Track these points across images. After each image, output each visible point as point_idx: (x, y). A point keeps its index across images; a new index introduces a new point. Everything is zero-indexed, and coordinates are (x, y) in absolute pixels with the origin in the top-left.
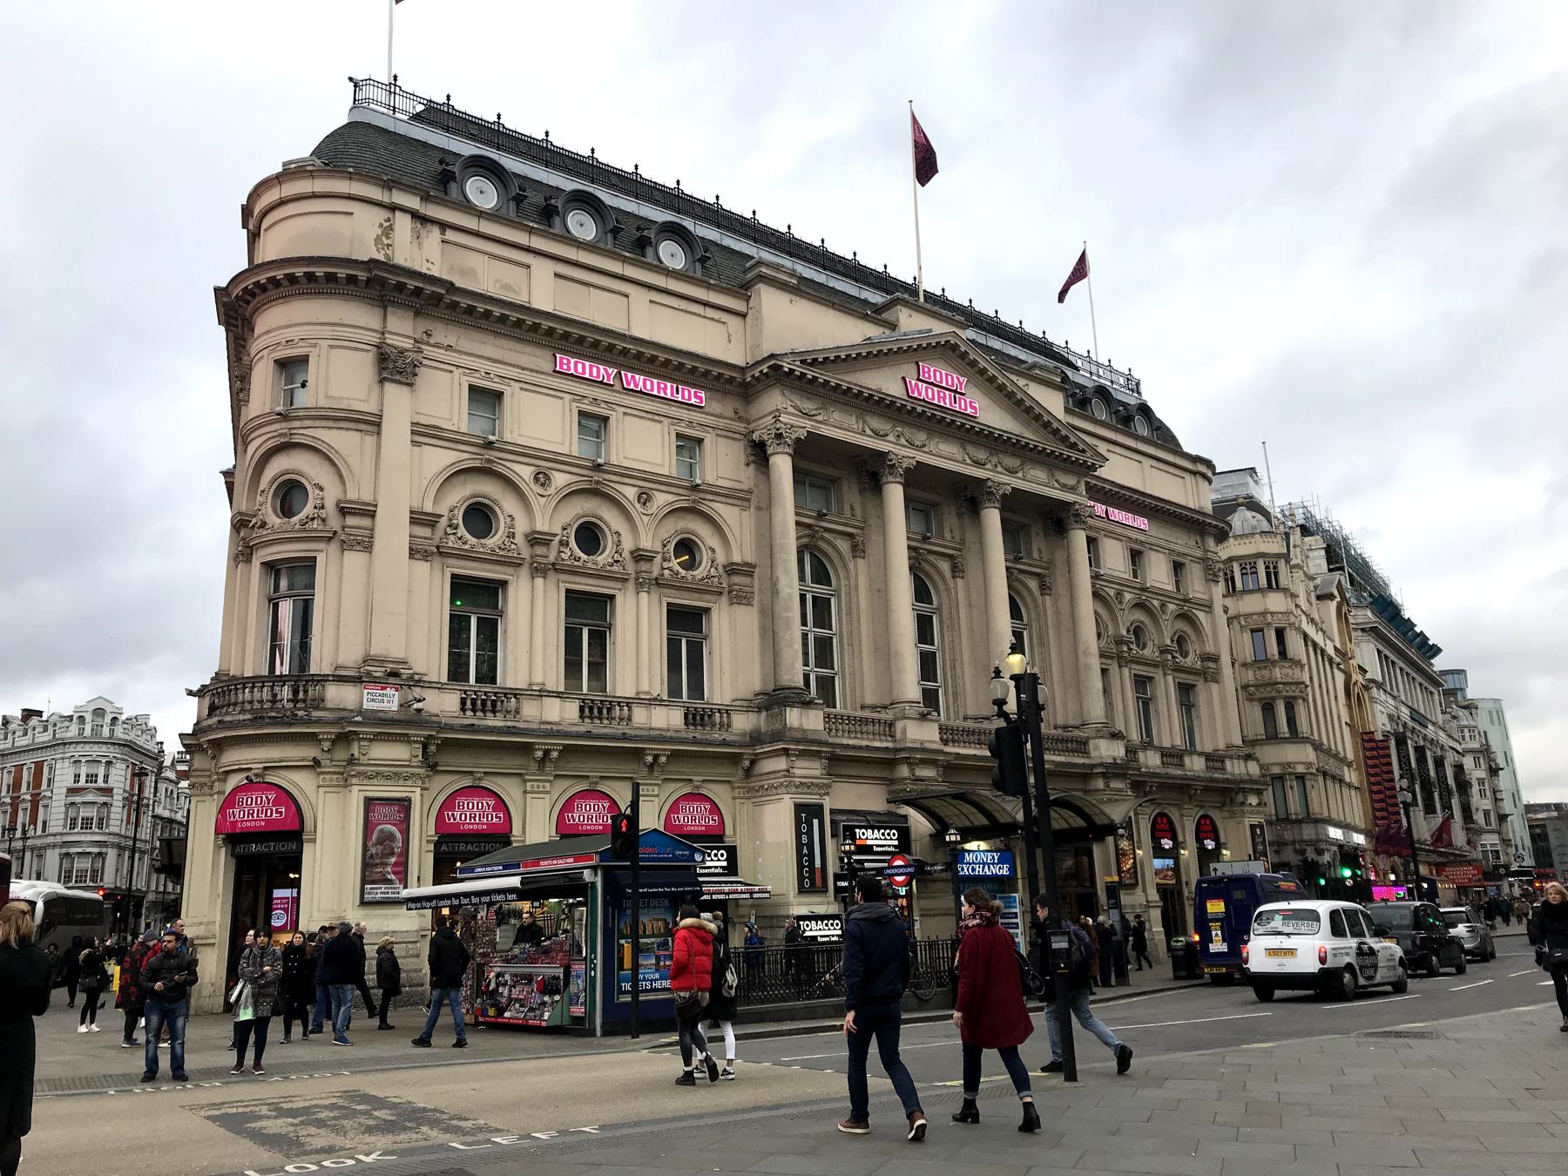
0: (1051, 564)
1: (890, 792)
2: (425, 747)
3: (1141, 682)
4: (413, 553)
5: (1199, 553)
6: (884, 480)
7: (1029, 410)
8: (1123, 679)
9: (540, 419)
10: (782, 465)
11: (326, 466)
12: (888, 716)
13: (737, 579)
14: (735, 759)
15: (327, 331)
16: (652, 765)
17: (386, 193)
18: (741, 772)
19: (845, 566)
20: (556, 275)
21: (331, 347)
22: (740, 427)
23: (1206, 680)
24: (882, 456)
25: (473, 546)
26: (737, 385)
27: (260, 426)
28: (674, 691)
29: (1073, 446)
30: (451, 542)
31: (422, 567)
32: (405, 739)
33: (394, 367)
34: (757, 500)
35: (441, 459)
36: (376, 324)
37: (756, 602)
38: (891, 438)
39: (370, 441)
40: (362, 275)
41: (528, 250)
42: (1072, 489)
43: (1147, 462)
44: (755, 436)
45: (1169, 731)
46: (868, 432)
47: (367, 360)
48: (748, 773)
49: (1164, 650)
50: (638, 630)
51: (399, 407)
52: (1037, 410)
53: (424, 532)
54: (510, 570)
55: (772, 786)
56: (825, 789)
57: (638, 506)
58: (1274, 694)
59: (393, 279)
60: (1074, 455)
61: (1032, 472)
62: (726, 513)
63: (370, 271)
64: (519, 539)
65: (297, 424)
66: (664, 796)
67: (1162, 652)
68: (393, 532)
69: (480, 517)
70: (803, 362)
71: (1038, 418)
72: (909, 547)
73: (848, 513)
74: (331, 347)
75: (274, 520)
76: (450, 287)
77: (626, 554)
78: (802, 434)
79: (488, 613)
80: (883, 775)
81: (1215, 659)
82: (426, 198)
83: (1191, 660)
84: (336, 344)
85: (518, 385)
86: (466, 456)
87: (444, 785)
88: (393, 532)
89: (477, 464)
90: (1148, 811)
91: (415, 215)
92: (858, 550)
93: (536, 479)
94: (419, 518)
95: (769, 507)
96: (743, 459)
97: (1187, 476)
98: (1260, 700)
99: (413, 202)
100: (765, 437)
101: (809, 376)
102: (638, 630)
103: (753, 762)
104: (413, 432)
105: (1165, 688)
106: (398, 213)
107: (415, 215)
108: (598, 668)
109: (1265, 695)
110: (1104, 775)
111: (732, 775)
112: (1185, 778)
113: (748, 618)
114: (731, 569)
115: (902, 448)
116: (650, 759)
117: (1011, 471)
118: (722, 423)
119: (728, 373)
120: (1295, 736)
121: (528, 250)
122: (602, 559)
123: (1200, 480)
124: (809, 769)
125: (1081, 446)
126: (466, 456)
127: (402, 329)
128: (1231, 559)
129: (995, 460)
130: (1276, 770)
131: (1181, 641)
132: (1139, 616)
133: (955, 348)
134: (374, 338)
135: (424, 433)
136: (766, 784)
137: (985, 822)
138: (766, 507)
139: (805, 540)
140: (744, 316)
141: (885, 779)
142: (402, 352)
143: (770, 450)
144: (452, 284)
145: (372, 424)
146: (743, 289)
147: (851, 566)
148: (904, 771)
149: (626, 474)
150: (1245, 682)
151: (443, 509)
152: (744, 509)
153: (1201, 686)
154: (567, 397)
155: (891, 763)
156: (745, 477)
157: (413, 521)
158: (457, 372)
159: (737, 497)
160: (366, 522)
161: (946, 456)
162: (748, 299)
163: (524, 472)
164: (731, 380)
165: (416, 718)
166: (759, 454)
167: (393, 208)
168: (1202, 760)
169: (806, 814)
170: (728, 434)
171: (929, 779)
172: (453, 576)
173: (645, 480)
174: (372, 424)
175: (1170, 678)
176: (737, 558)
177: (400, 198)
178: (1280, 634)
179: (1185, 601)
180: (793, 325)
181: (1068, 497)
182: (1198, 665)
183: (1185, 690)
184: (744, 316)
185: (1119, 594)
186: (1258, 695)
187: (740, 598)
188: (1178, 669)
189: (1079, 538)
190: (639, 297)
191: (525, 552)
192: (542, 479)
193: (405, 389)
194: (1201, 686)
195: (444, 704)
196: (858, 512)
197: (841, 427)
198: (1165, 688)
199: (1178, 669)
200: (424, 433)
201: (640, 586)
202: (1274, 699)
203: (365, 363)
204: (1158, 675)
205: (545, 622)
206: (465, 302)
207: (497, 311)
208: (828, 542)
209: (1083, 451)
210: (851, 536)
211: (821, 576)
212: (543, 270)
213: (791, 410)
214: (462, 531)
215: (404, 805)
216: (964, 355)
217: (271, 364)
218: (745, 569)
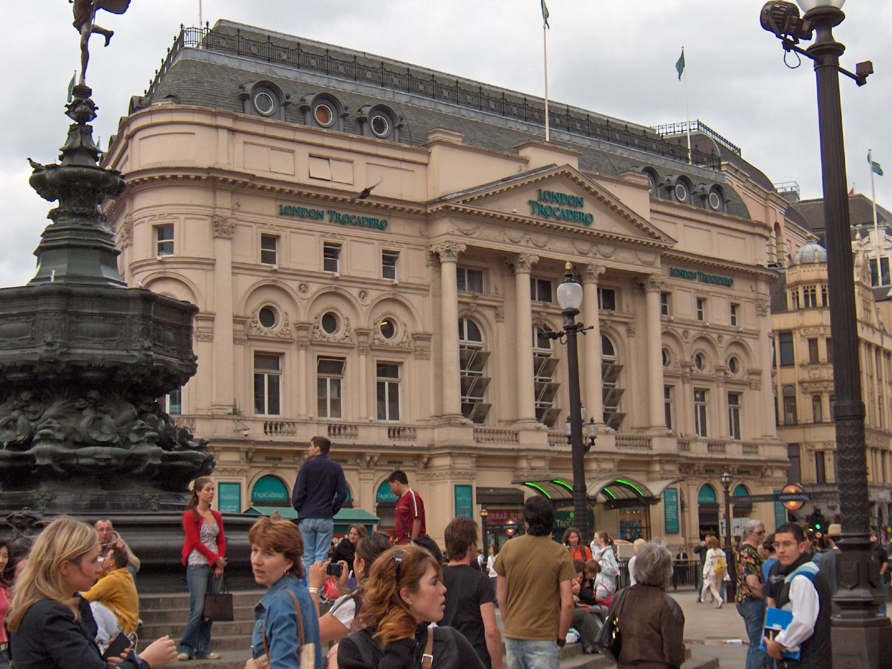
0: (634, 316)
1: (515, 476)
2: (247, 453)
3: (701, 394)
4: (235, 340)
5: (753, 295)
6: (517, 271)
7: (620, 212)
8: (684, 393)
9: (301, 248)
10: (449, 270)
11: (185, 290)
12: (515, 427)
13: (419, 343)
14: (418, 457)
15: (183, 209)
16: (369, 463)
17: (213, 118)
18: (422, 465)
19: (490, 327)
20: (311, 156)
21: (186, 218)
22: (422, 241)
23: (751, 388)
24: (516, 255)
25: (266, 334)
26: (423, 214)
27: (141, 266)
28: (381, 416)
29: (651, 235)
30: (254, 332)
31: (240, 348)
32: (237, 450)
33: (222, 229)
35: (248, 282)
36: (210, 202)
37: (432, 357)
38: (523, 243)
39: (210, 274)
40: (204, 176)
41: (293, 141)
42: (650, 264)
43: (715, 230)
44: (433, 249)
45: (718, 427)
46: (576, 253)
47: (206, 225)
48: (427, 466)
50: (359, 375)
52: (626, 212)
53: (240, 327)
54: (286, 346)
55: (441, 474)
56: (472, 476)
57: (359, 300)
58: (821, 389)
59: (221, 177)
60: (657, 242)
61: (621, 255)
62: (413, 300)
63: (208, 173)
64: (291, 327)
65: (169, 266)
66: (376, 480)
67: (717, 370)
69: (268, 315)
70: (464, 202)
71: (627, 217)
72: (533, 312)
73: (493, 291)
74: (186, 218)
76: (253, 177)
77: (353, 331)
78: (463, 248)
79: (274, 372)
80: (510, 465)
81: (758, 373)
82: (236, 119)
83: (740, 375)
84: (189, 216)
85: (289, 230)
86: (261, 279)
87: (257, 473)
89: (391, 296)
90: (697, 483)
91: (232, 131)
92: (499, 317)
93: (300, 288)
94: (237, 320)
95: (440, 296)
96: (424, 262)
98: (811, 393)
99: (229, 123)
100: (439, 250)
101: (465, 208)
102: (359, 375)
103: (429, 459)
104: (233, 268)
105: (717, 398)
106: (220, 131)
107: (232, 131)
108: (336, 403)
109: (815, 389)
110: (660, 462)
111: (416, 466)
112: (726, 460)
114: (417, 337)
116: (368, 458)
117: (606, 257)
118: (411, 240)
119: (415, 209)
121: (293, 141)
122: (338, 335)
123: (757, 239)
124: (465, 464)
125: (657, 234)
126: (261, 279)
127: (224, 201)
128: (798, 283)
129: (595, 249)
130: (819, 447)
131: (733, 362)
132: (702, 345)
133: (569, 175)
134: (209, 211)
135: (237, 268)
136: (437, 473)
138: (438, 294)
139: (464, 313)
140: (426, 165)
141: (512, 468)
142: (225, 219)
143: (442, 260)
144: (254, 176)
145: (208, 264)
146: (425, 147)
147: (495, 328)
148: (524, 464)
149: (351, 280)
150: (801, 378)
151: (249, 313)
152: (425, 296)
153: (746, 392)
154: (376, 242)
155: (516, 459)
156: (425, 275)
157: (235, 322)
158: (255, 226)
159: (421, 289)
160: (208, 324)
162: (429, 154)
163: (293, 285)
164: (418, 212)
165: (245, 438)
167: (217, 127)
168: (740, 447)
169: (461, 490)
171: (540, 468)
172: (255, 352)
173: (363, 283)
175: (721, 389)
176: (420, 329)
179: (738, 332)
180: (456, 171)
182: (746, 378)
183: (733, 398)
184: (426, 165)
185: (686, 332)
186: (810, 389)
187: (422, 355)
188: (728, 382)
189: (654, 299)
190: (360, 161)
191: (295, 335)
192: (303, 288)
193: (228, 243)
194: (746, 392)
195: (257, 432)
196: (500, 292)
197: (490, 239)
198: (717, 398)
199: (728, 382)
201: (362, 351)
202: (821, 392)
203: (203, 228)
204: (713, 387)
205: (307, 377)
206: (259, 184)
207: (278, 187)
208: (480, 313)
209: (659, 238)
210: (495, 307)
211: (475, 334)
212: (302, 152)
213: (456, 232)
214: (260, 325)
215: (239, 484)
216: (575, 179)
217: (150, 229)
218: (425, 337)
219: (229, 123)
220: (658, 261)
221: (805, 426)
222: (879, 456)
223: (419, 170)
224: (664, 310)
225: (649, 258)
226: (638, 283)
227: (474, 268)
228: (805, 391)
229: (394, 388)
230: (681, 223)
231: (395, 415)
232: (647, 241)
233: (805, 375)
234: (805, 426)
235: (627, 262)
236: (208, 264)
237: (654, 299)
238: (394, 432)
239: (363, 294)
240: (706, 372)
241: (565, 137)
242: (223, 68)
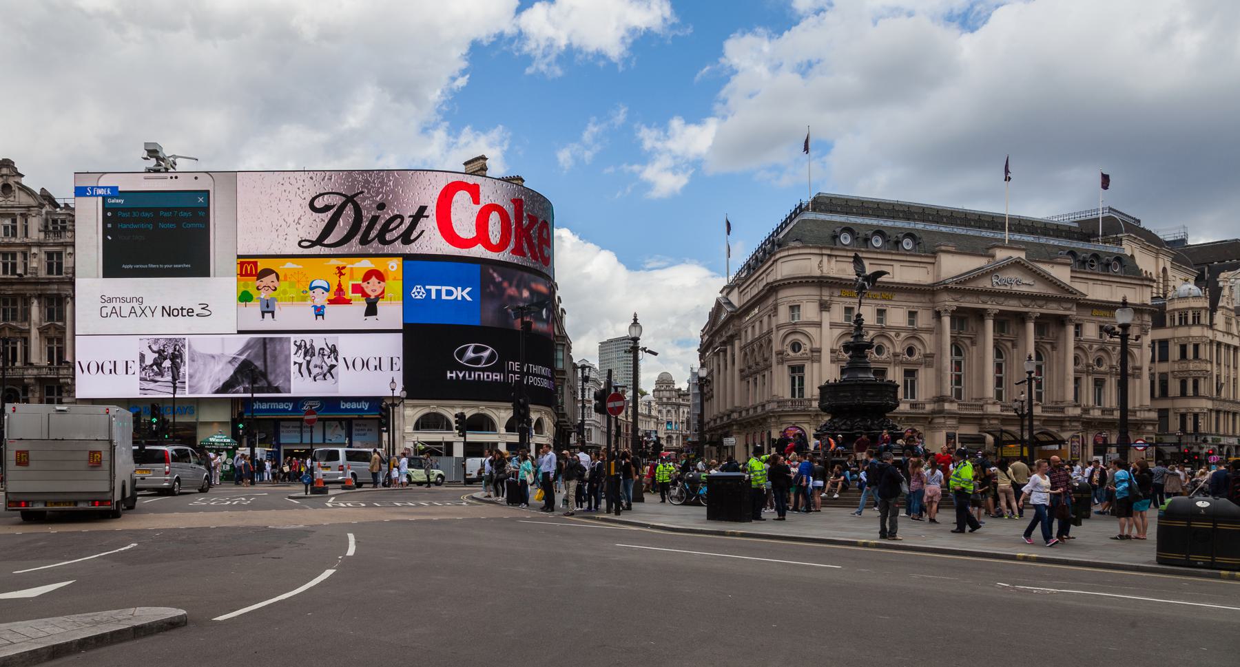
10: (947, 320)
29: (1071, 293)
33: (824, 306)
34: (937, 331)
42: (1069, 309)
49: (1111, 367)
51: (826, 318)
68: (826, 356)
75: (792, 354)
88: (826, 356)
91: (829, 256)
97: (1138, 288)
99: (828, 252)
101: (960, 286)
107: (829, 256)
113: (931, 372)
114: (926, 356)
115: (993, 306)
120: (1196, 395)
130: (1183, 411)
135: (833, 325)
137: (326, 242)
146: (934, 254)
161: (1012, 306)
166: (938, 315)
170: (927, 309)
174: (819, 325)
177: (824, 252)
178: (1196, 347)
180: (953, 266)
181: (1067, 313)
187: (928, 365)
189: (1071, 329)
200: (833, 325)
204: (1107, 378)
218: (931, 356)
219: (828, 252)
220: (1074, 308)
221: (1174, 398)
222: (1231, 417)
223: (930, 267)
224: (1077, 334)
225: (1069, 306)
226: (1061, 321)
227: (961, 317)
228: (1175, 377)
229: (802, 379)
230: (1091, 283)
231: (913, 396)
232: (1067, 295)
233: (1176, 367)
234: (1174, 398)
235: (1053, 309)
236: (819, 325)
237: (1071, 329)
238: (1103, 411)
239: (897, 335)
240: (1102, 369)
241: (1017, 237)
242: (823, 221)
